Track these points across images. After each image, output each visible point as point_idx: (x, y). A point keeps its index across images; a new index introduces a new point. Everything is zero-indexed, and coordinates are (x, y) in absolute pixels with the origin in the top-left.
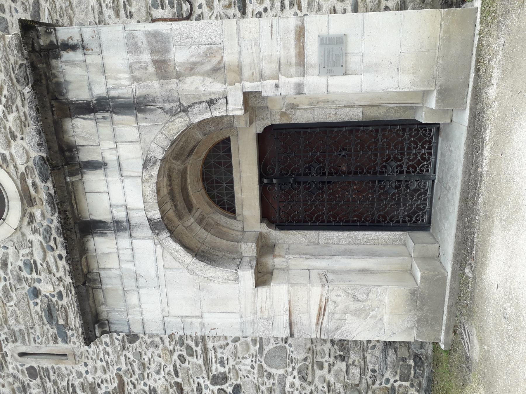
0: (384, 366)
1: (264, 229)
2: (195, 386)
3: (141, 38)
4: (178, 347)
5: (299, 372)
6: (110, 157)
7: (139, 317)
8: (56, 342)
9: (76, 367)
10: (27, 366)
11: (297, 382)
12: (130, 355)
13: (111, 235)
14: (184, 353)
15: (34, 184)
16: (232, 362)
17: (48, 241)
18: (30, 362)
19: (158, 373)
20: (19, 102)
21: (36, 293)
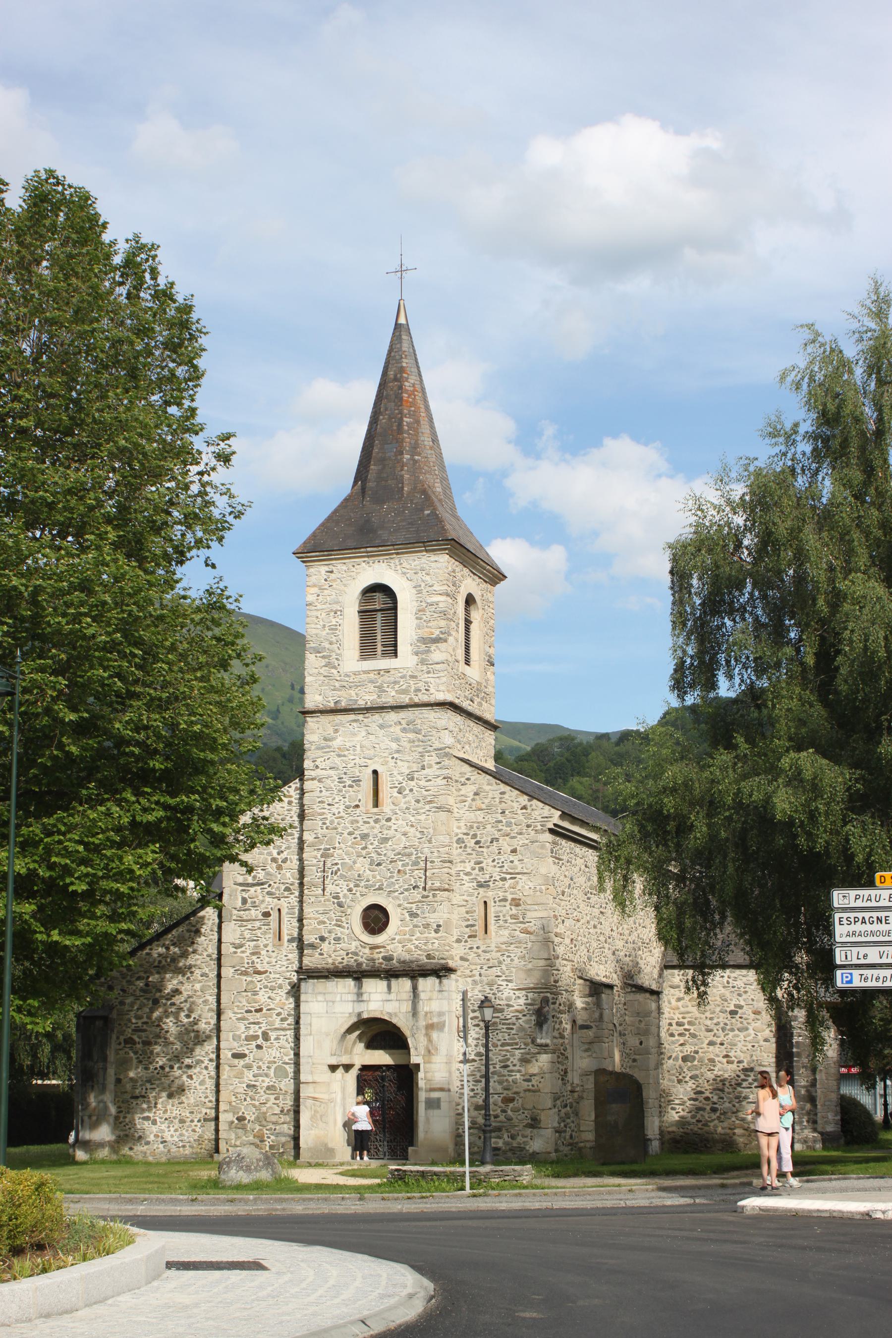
0: (277, 1135)
1: (358, 1066)
2: (260, 1020)
3: (443, 1019)
4: (286, 1013)
5: (273, 1086)
6: (393, 996)
7: (310, 999)
8: (288, 935)
9: (271, 945)
10: (271, 912)
11: (265, 1084)
12: (280, 981)
13: (355, 990)
14: (282, 1016)
15: (381, 952)
16: (277, 1045)
17: (352, 953)
18: (274, 915)
19: (269, 998)
20: (419, 952)
21: (322, 939)
